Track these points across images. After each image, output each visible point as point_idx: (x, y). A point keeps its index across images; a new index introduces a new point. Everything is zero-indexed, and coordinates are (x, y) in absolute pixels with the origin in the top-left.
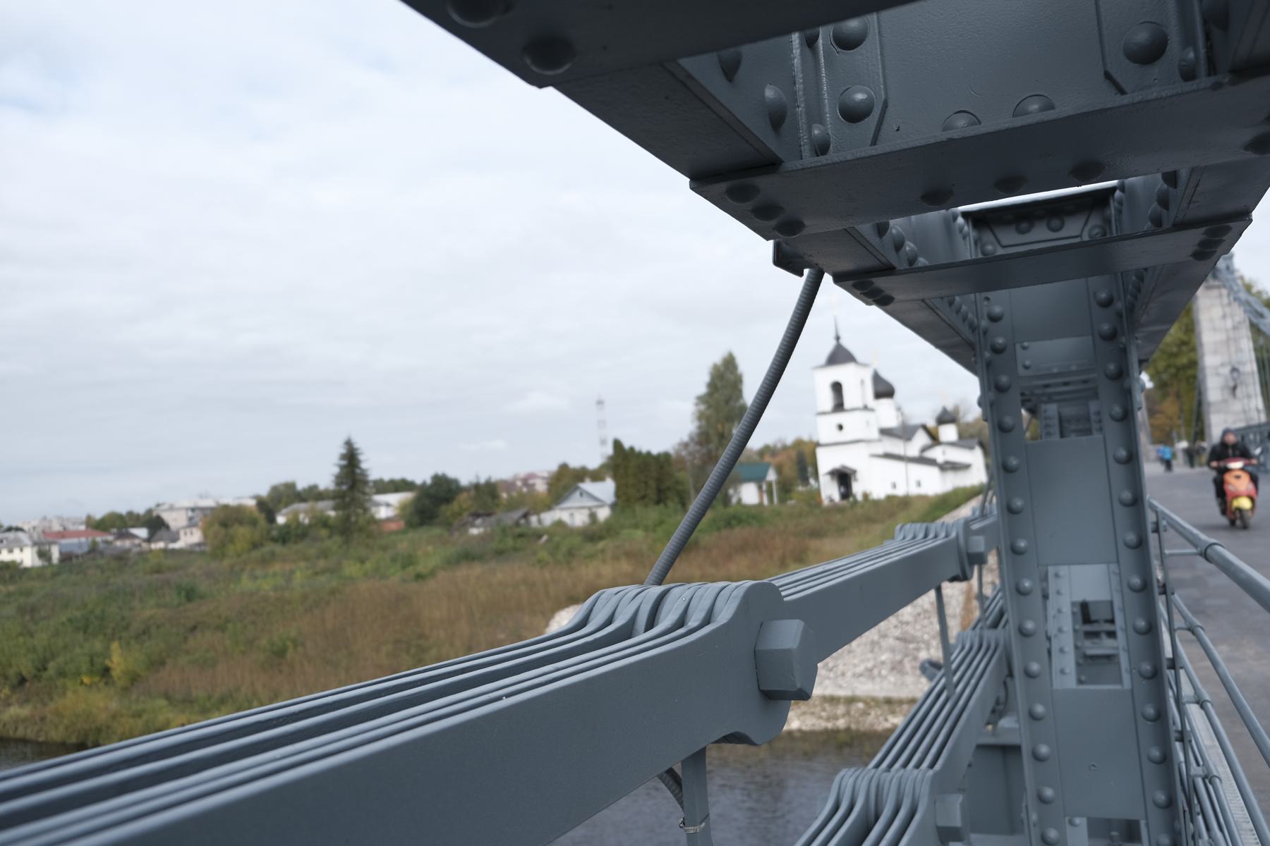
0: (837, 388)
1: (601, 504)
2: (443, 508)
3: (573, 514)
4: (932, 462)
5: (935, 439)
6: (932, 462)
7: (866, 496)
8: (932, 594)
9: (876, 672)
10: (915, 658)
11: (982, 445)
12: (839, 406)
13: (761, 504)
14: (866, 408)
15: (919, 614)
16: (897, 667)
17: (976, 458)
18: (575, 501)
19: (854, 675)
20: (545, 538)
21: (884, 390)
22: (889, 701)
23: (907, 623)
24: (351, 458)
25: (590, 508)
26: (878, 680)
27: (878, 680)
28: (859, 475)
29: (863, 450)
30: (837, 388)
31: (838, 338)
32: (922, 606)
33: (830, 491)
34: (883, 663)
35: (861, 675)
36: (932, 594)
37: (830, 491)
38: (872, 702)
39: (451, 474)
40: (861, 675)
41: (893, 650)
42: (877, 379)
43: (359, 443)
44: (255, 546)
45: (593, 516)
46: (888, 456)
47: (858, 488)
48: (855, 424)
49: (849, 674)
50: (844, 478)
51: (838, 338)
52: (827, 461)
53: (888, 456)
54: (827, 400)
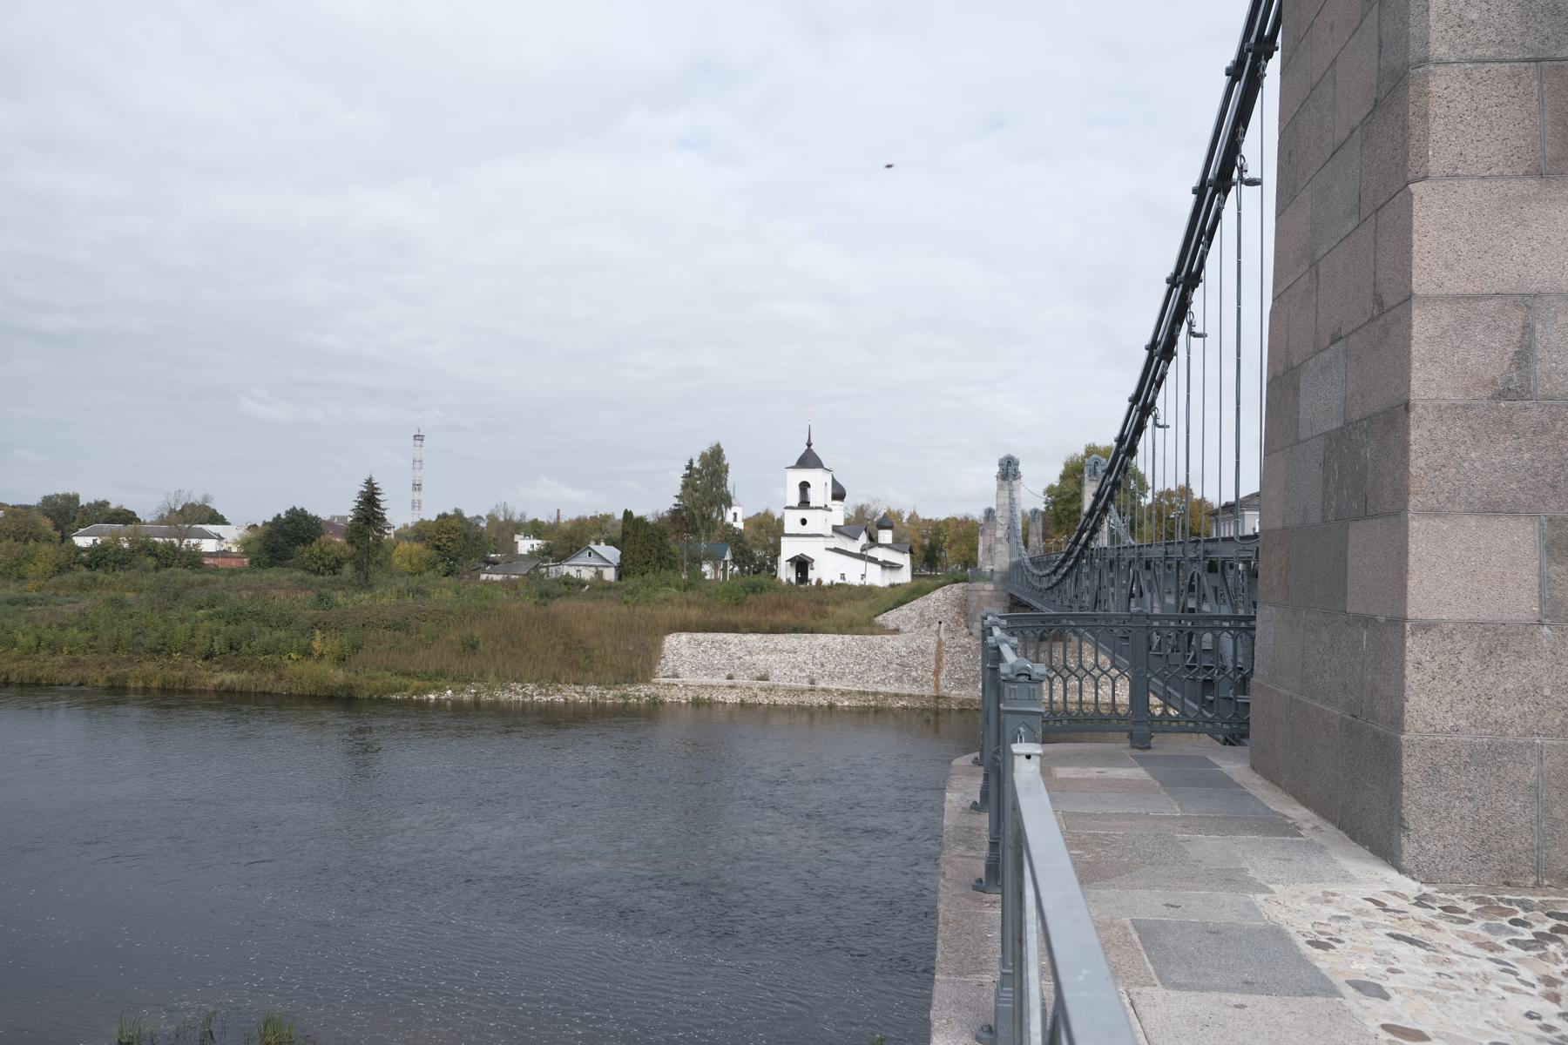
0: (804, 486)
1: (608, 563)
2: (300, 548)
3: (579, 569)
4: (874, 560)
5: (873, 541)
6: (874, 560)
7: (819, 581)
8: (1242, 495)
9: (887, 681)
10: (909, 676)
11: (911, 552)
12: (804, 503)
13: (716, 579)
14: (826, 508)
15: (911, 652)
16: (899, 679)
17: (904, 560)
18: (583, 559)
19: (874, 682)
20: (587, 587)
21: (839, 495)
22: (896, 695)
23: (904, 657)
24: (370, 500)
25: (596, 567)
26: (888, 685)
27: (888, 685)
28: (815, 564)
29: (821, 544)
30: (804, 486)
31: (809, 445)
32: (912, 648)
33: (786, 573)
34: (891, 677)
35: (878, 683)
36: (1242, 495)
37: (786, 573)
38: (887, 695)
39: (312, 511)
40: (878, 683)
41: (896, 671)
42: (835, 483)
43: (380, 482)
44: (61, 569)
45: (599, 574)
46: (837, 550)
47: (813, 575)
48: (819, 522)
49: (871, 682)
50: (802, 564)
51: (809, 445)
52: (789, 549)
53: (837, 550)
54: (795, 499)
